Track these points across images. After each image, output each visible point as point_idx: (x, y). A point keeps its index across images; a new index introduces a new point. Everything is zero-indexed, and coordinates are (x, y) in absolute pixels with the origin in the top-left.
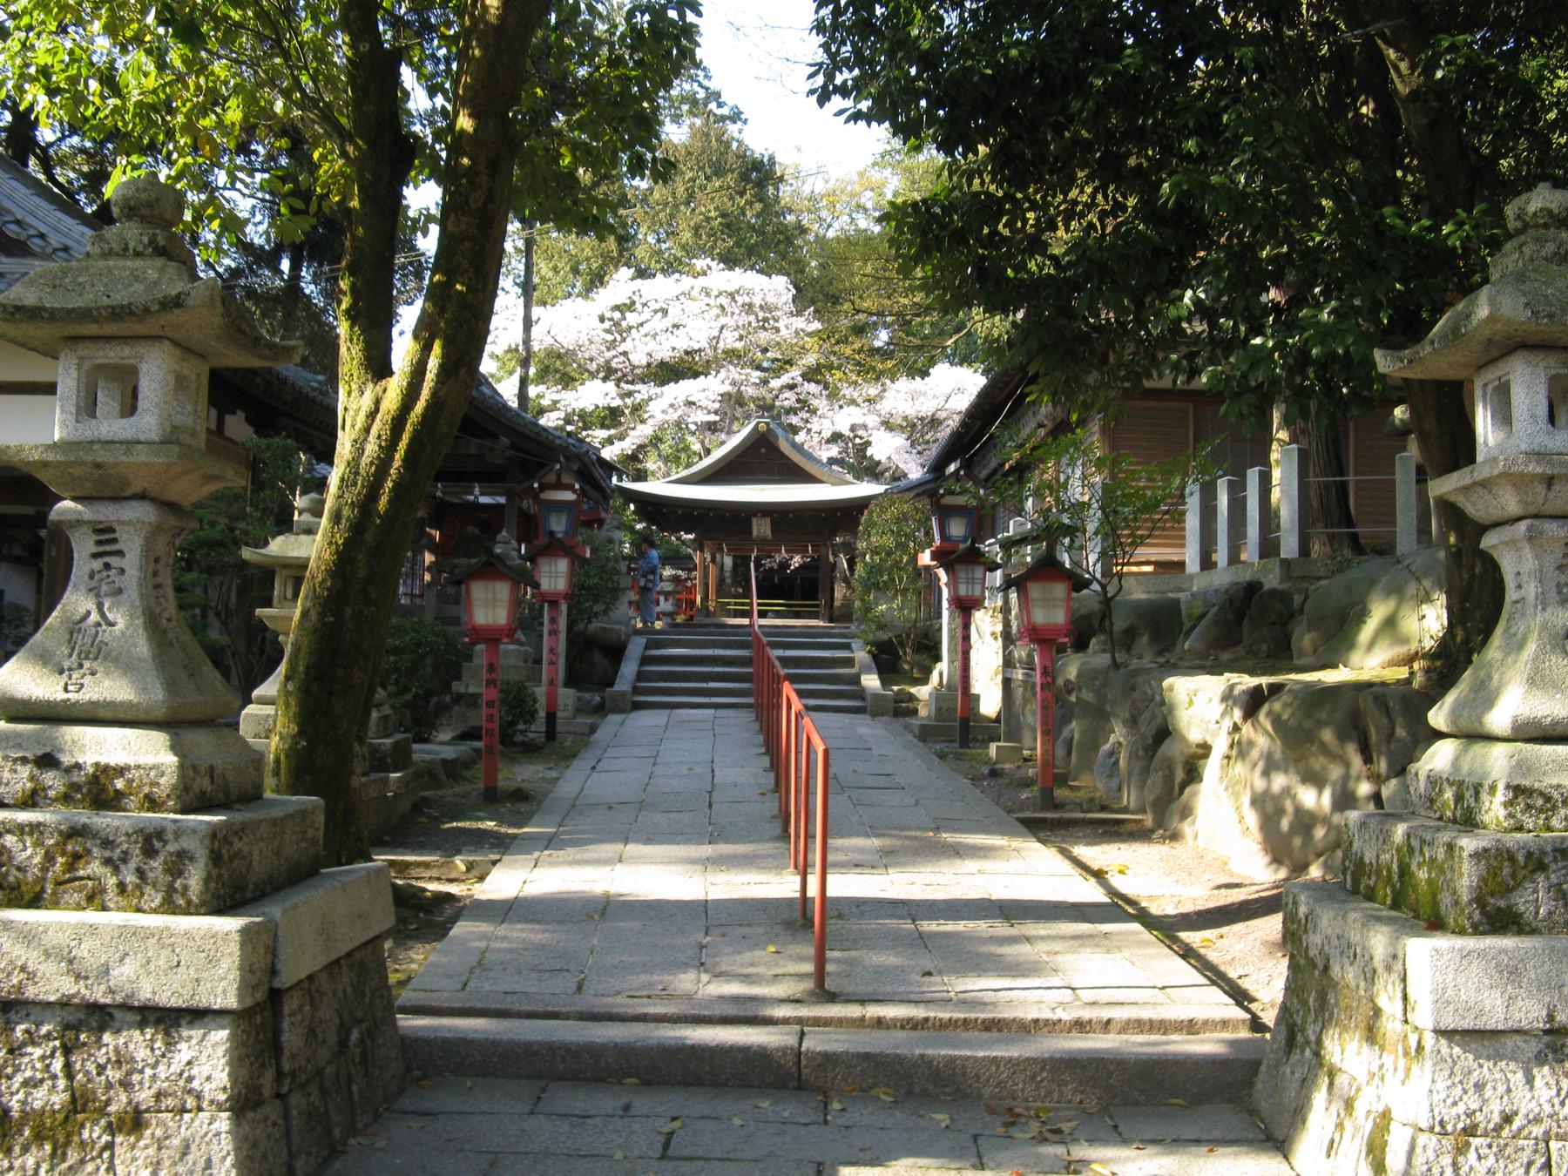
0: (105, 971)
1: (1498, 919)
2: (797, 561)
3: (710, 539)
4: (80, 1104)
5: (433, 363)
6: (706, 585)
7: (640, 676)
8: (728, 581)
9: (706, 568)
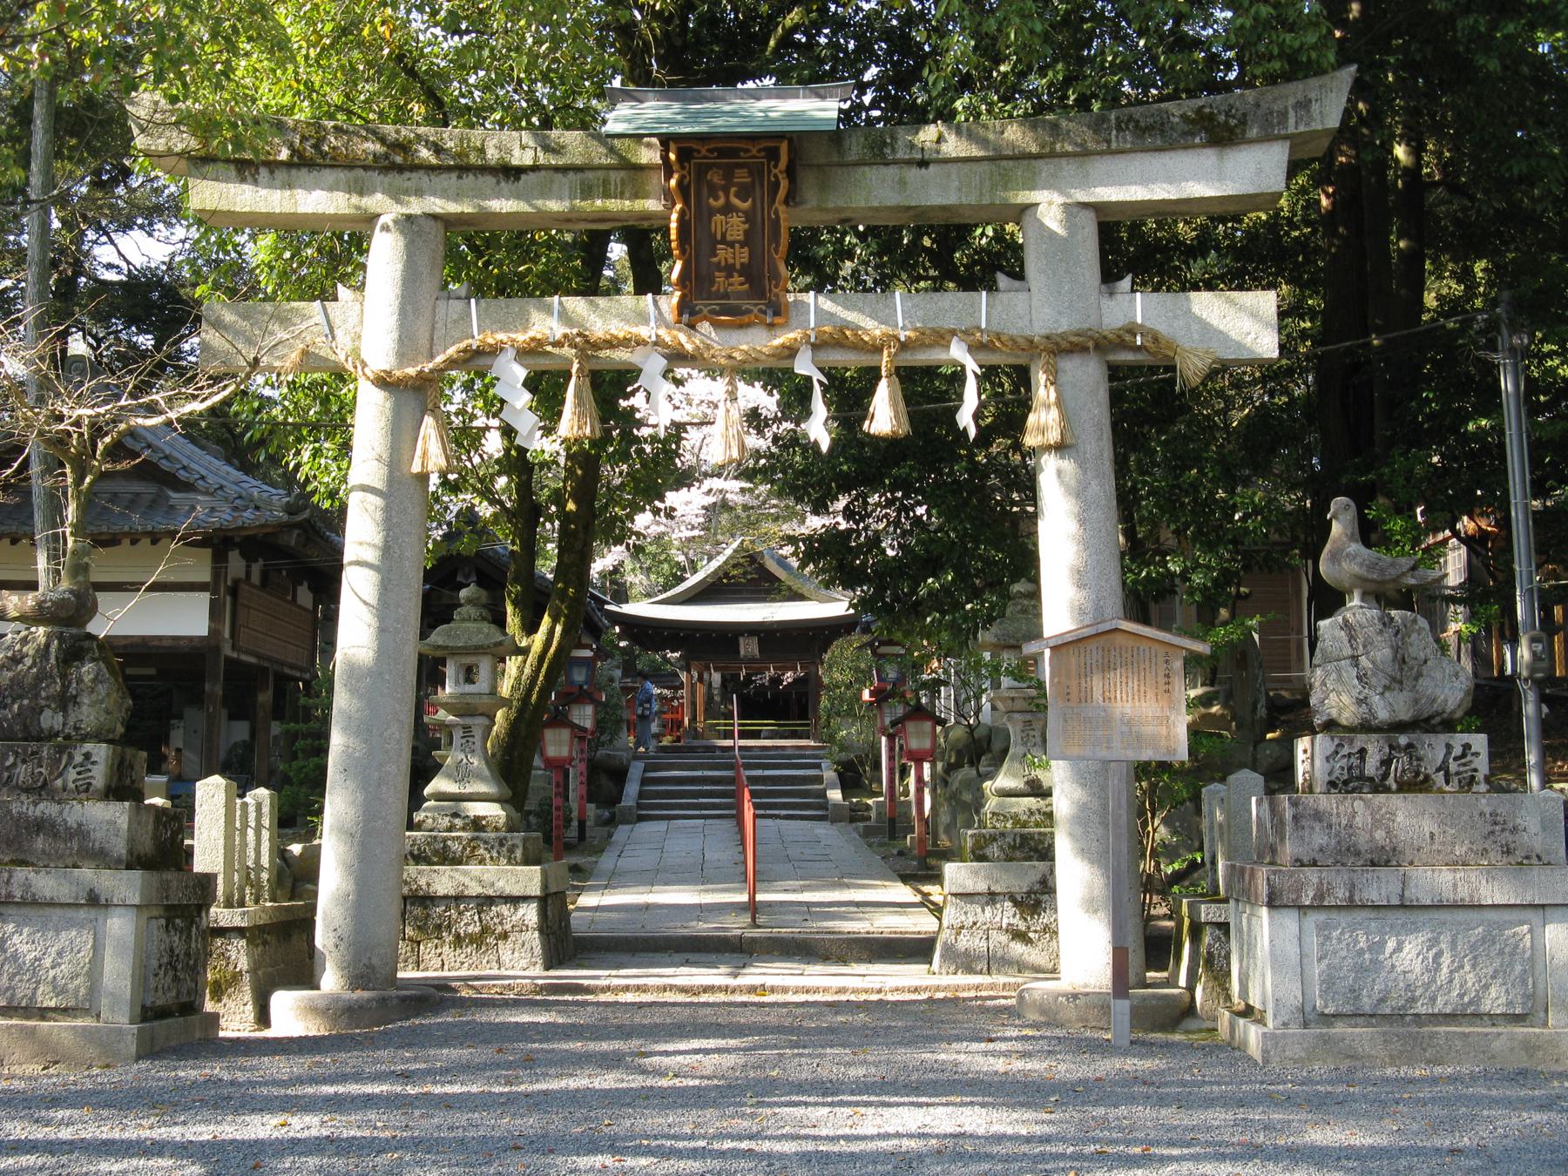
0: (493, 884)
1: (981, 858)
2: (789, 677)
3: (698, 659)
4: (485, 930)
5: (559, 629)
6: (694, 704)
7: (641, 795)
8: (717, 698)
9: (693, 686)
